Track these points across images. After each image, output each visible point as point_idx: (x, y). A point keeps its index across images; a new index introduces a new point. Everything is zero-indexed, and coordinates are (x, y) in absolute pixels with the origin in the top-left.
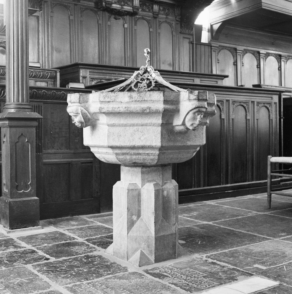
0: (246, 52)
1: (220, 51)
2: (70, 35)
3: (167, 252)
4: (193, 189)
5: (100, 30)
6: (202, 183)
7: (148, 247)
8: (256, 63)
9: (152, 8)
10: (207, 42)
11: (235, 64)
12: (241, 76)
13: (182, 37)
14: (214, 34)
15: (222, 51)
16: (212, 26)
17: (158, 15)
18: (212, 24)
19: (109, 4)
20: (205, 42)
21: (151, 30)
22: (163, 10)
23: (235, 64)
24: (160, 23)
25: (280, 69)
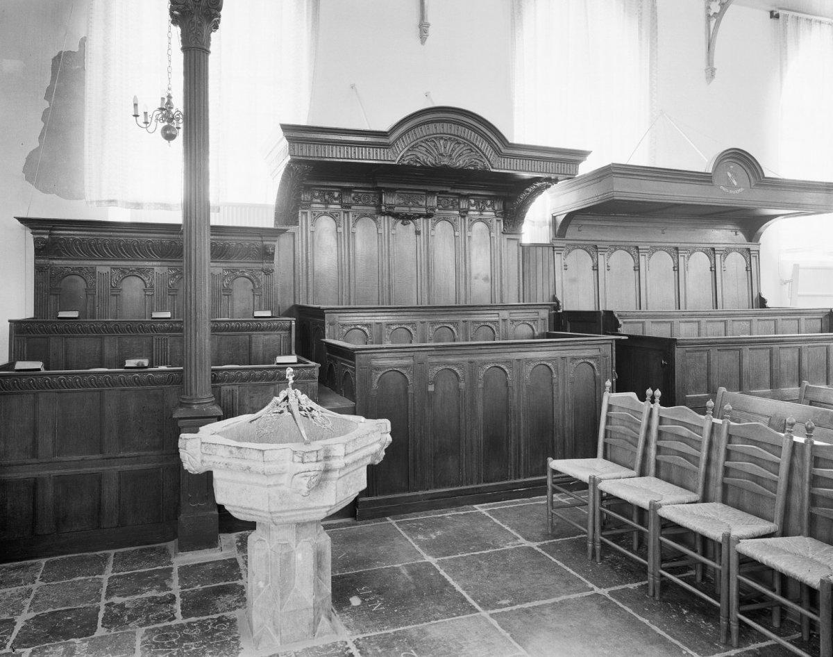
0: (654, 249)
1: (569, 252)
2: (428, 254)
3: (299, 632)
4: (465, 487)
5: (304, 240)
6: (522, 474)
7: (274, 625)
8: (631, 263)
9: (459, 204)
10: (548, 242)
11: (595, 268)
12: (685, 283)
13: (506, 240)
14: (557, 229)
15: (574, 252)
16: (554, 218)
17: (466, 212)
18: (554, 215)
19: (390, 208)
20: (545, 242)
21: (457, 234)
22: (475, 205)
23: (713, 269)
24: (472, 222)
25: (676, 269)
